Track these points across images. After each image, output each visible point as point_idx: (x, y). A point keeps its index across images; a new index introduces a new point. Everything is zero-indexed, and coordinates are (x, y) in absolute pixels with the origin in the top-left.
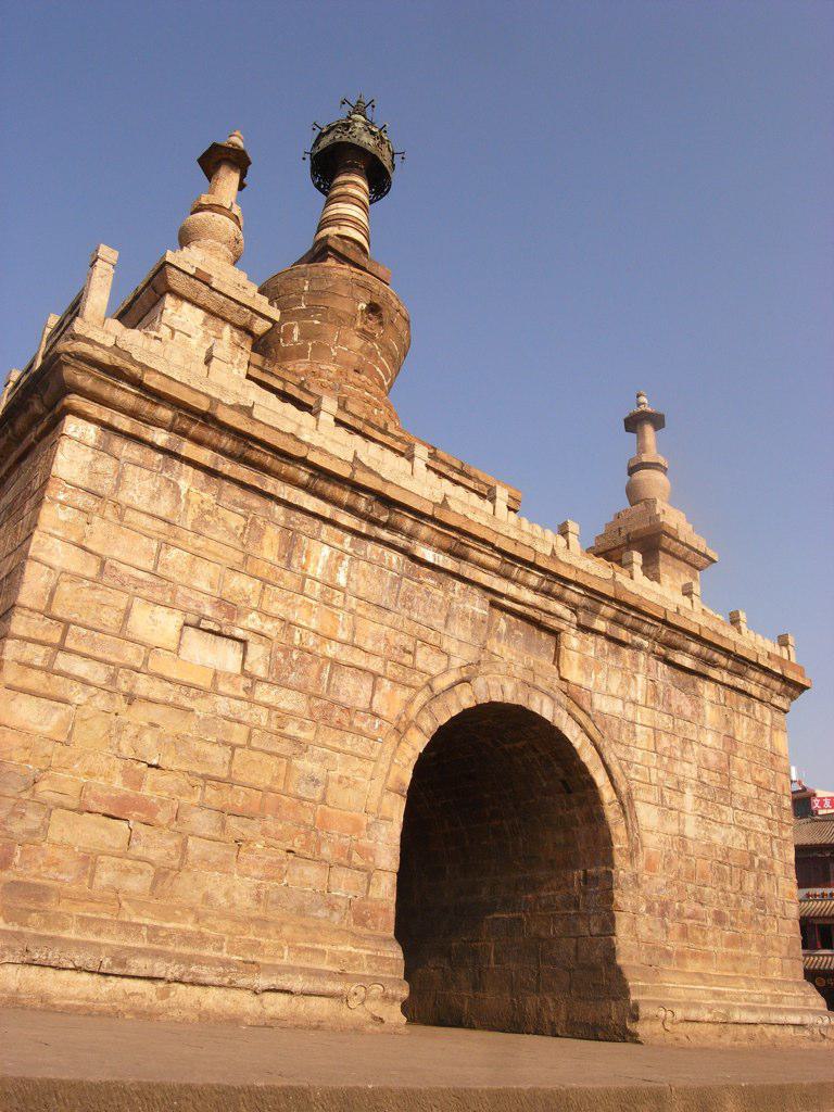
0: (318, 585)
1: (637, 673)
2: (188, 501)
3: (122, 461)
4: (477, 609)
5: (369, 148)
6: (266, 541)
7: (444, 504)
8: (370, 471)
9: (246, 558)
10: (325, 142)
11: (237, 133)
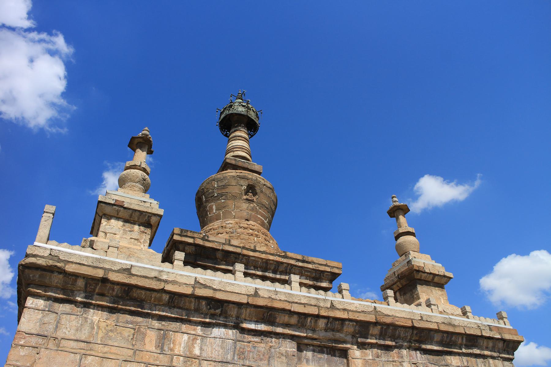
0: (182, 358)
1: (403, 362)
2: (99, 327)
3: (59, 314)
4: (288, 349)
5: (242, 113)
6: (147, 340)
7: (256, 294)
8: (205, 286)
9: (135, 352)
10: (223, 116)
11: (146, 128)
